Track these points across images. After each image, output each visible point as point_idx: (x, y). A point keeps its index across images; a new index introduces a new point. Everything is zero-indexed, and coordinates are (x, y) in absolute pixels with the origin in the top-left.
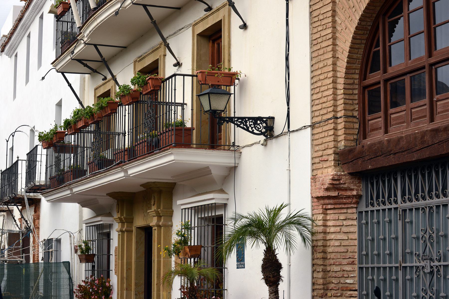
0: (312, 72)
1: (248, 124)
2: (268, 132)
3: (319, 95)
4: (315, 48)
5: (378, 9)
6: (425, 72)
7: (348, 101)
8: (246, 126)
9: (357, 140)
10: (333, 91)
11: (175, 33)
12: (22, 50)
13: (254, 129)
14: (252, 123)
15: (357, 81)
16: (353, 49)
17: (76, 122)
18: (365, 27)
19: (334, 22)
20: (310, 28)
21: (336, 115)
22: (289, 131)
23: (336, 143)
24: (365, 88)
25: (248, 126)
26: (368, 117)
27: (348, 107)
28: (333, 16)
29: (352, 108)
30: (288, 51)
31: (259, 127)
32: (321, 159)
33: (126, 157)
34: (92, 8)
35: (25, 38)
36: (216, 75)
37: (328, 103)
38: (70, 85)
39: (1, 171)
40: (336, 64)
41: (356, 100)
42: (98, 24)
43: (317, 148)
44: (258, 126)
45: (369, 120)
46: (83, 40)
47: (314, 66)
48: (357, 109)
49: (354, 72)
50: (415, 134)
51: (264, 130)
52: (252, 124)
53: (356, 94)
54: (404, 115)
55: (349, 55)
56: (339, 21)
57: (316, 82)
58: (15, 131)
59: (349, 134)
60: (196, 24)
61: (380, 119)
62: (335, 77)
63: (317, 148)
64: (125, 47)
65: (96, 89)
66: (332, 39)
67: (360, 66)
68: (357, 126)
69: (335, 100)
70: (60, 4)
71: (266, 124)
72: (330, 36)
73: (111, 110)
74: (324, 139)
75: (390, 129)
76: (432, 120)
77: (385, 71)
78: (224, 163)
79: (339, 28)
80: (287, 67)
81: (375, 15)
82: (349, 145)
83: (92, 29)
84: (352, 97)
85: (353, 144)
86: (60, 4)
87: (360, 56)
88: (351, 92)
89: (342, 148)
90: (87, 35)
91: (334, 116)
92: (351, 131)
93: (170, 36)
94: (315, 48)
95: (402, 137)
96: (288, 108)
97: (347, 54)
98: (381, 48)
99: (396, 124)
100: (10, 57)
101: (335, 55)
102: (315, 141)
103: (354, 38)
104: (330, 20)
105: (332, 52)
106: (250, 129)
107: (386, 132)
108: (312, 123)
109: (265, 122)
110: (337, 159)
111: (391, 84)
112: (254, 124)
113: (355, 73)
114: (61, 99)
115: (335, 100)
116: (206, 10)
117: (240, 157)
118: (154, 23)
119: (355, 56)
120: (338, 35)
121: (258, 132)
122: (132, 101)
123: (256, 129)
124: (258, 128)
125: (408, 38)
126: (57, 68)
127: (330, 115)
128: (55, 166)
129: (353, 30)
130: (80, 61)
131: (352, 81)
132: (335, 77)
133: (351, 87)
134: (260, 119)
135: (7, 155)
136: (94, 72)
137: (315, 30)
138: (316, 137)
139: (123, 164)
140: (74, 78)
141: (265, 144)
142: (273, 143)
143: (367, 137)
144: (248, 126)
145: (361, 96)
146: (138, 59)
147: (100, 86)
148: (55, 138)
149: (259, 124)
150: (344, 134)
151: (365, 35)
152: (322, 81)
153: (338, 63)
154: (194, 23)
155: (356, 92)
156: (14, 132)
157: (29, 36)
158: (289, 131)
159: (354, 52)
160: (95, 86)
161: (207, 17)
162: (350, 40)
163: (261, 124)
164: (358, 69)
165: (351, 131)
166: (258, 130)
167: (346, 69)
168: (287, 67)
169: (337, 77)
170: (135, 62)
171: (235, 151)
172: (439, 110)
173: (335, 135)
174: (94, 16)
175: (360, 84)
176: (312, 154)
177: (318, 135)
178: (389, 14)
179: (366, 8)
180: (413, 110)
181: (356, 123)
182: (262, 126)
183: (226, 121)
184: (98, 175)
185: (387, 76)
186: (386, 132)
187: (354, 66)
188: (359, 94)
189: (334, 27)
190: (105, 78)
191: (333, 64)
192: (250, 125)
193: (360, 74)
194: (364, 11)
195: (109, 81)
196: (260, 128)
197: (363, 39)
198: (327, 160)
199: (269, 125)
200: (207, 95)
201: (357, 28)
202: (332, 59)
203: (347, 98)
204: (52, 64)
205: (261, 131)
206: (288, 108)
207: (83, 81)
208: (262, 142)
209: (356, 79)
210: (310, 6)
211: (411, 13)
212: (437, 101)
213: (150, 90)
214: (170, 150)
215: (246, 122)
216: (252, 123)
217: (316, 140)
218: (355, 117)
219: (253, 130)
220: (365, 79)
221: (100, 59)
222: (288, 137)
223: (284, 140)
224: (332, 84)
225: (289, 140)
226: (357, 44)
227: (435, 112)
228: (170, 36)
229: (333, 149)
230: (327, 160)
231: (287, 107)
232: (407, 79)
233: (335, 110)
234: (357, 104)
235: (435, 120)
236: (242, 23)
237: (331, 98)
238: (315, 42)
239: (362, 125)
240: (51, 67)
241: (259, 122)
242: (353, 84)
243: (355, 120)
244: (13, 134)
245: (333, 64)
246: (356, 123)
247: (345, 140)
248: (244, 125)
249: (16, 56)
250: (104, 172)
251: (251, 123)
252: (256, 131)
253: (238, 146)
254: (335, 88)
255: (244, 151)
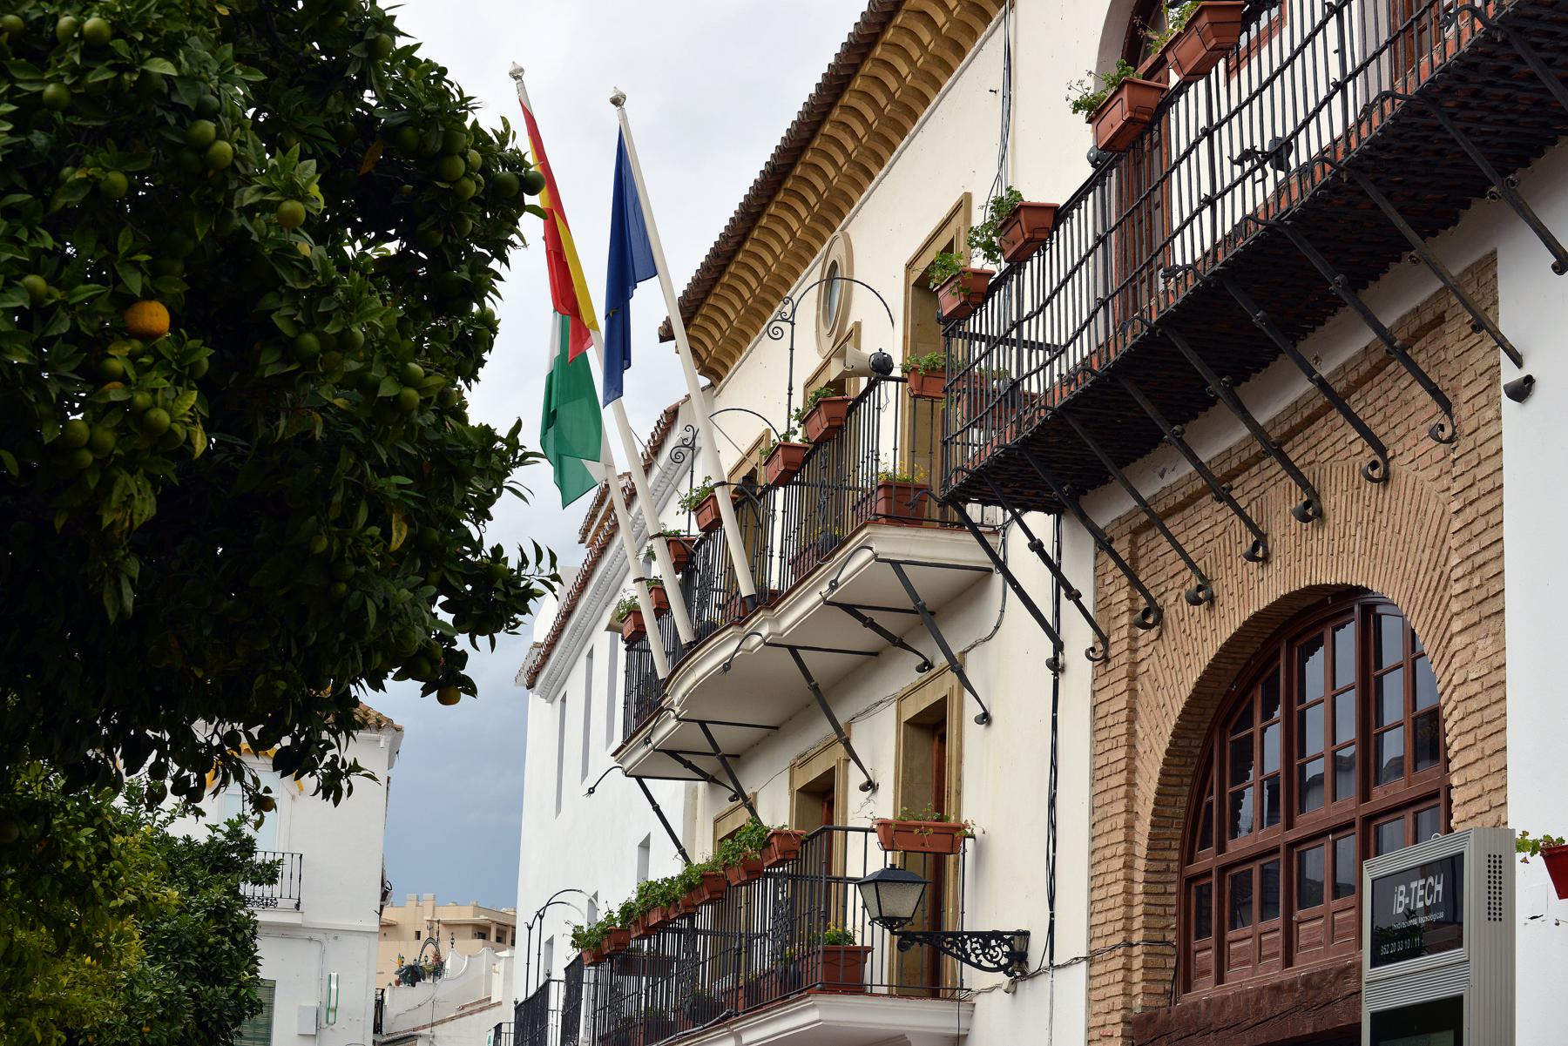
0: (1093, 839)
1: (968, 947)
2: (1016, 964)
3: (1103, 891)
4: (1101, 787)
5: (1212, 712)
6: (1439, 805)
7: (1153, 909)
8: (964, 951)
9: (1172, 993)
10: (1125, 886)
11: (867, 711)
12: (575, 687)
13: (981, 957)
14: (978, 945)
15: (1174, 866)
16: (1163, 797)
17: (645, 914)
18: (1186, 750)
19: (1131, 734)
20: (1092, 742)
21: (1131, 938)
22: (1051, 965)
23: (1127, 998)
24: (1191, 880)
25: (969, 951)
26: (1195, 945)
27: (1154, 922)
28: (1131, 721)
29: (1162, 923)
30: (1055, 788)
31: (995, 954)
32: (1101, 1031)
33: (741, 1003)
34: (683, 642)
35: (583, 659)
36: (916, 831)
37: (1117, 910)
38: (657, 809)
39: (516, 1003)
40: (1133, 827)
41: (1172, 906)
42: (697, 681)
43: (1097, 1008)
44: (992, 952)
45: (1196, 952)
46: (760, 635)
47: (1096, 826)
48: (1174, 926)
49: (1167, 846)
50: (1247, 992)
51: (1004, 961)
52: (977, 948)
53: (1171, 894)
54: (1250, 946)
55: (1154, 810)
56: (1141, 734)
57: (1098, 862)
58: (548, 905)
59: (1154, 980)
60: (903, 697)
61: (1210, 952)
62: (1130, 855)
63: (1097, 1008)
64: (776, 728)
65: (717, 821)
66: (1125, 772)
67: (1180, 832)
68: (1172, 962)
69: (1129, 905)
70: (629, 614)
71: (1011, 947)
72: (1122, 765)
73: (710, 894)
74: (1109, 988)
75: (1227, 974)
76: (1288, 962)
77: (1222, 849)
78: (935, 1028)
79: (1140, 749)
80: (1053, 825)
81: (1206, 726)
82: (1153, 1004)
83: (687, 691)
84: (1162, 900)
85: (1162, 1002)
86: (629, 614)
87: (1181, 812)
88: (1160, 888)
89: (1138, 1010)
90: (679, 702)
91: (1124, 941)
92: (1158, 975)
93: (858, 715)
94: (1101, 787)
95: (1227, 998)
96: (1052, 915)
97: (1152, 806)
98: (1214, 798)
99: (1237, 965)
100: (552, 702)
101: (1133, 806)
102: (1094, 993)
103: (1163, 773)
104: (1123, 729)
105: (1125, 801)
106: (973, 959)
107: (1220, 979)
108: (1091, 952)
109: (1007, 942)
110: (1130, 1033)
111: (1231, 876)
112: (983, 948)
113: (1170, 848)
114: (649, 835)
115: (1129, 905)
116: (920, 669)
117: (971, 1016)
118: (815, 688)
119: (1169, 812)
120: (1138, 763)
121: (991, 965)
122: (746, 878)
123: (986, 959)
124: (991, 956)
125: (1411, 721)
126: (627, 765)
127: (1118, 939)
128: (773, 934)
129: (1161, 755)
130: (850, 609)
131: (1163, 866)
132: (1130, 855)
133: (1162, 878)
134: (997, 935)
135: (539, 954)
136: (895, 645)
137: (1100, 749)
138: (1096, 982)
139: (734, 1018)
140: (671, 793)
141: (1012, 990)
142: (1025, 987)
143: (1193, 988)
144: (969, 951)
145: (1182, 897)
146: (798, 762)
147: (726, 815)
148: (606, 944)
149: (993, 948)
150: (1143, 980)
151: (1190, 766)
152: (1109, 862)
153: (1138, 826)
154: (899, 695)
155: (1173, 888)
156: (545, 908)
157: (590, 655)
158: (1051, 965)
159: (1166, 803)
160: (715, 814)
161: (923, 684)
162: (1156, 776)
163: (999, 946)
164: (1176, 839)
165: (1158, 975)
166: (991, 961)
167: (1150, 839)
168: (1053, 825)
169: (1134, 855)
170: (792, 767)
171: (960, 1000)
172: (1302, 942)
173: (1127, 981)
174: (689, 662)
175: (1180, 872)
176: (1088, 1021)
177: (1099, 979)
178: (1231, 727)
179: (1183, 711)
180: (1263, 938)
181: (1171, 956)
182: (1001, 953)
183: (919, 940)
184: (686, 1040)
185: (1224, 859)
186: (1220, 979)
187: (1168, 833)
188: (1179, 892)
189: (1131, 746)
190: (927, 665)
191: (1126, 827)
192: (973, 950)
193: (1181, 850)
194: (1180, 717)
195: (942, 672)
196: (997, 956)
197: (1186, 776)
198: (1112, 1036)
199: (1017, 949)
200: (873, 885)
201: (1168, 752)
202: (1124, 814)
203: (1153, 901)
204: (614, 754)
205: (998, 963)
206: (1052, 915)
207: (692, 797)
208: (1005, 986)
209: (1173, 861)
210: (1094, 693)
211: (1338, 695)
212: (1299, 923)
213: (775, 859)
214: (810, 999)
215: (964, 942)
216: (978, 945)
217: (1096, 989)
218: (1168, 943)
219: (980, 961)
220: (1190, 861)
221: (910, 605)
222: (1050, 978)
223: (1043, 982)
224: (1123, 871)
225: (1052, 986)
226: (1175, 786)
227: (1295, 946)
228: (858, 715)
229: (1122, 1012)
230: (1112, 1036)
231: (1048, 912)
232: (1256, 868)
233: (1128, 926)
234: (1175, 915)
235: (1295, 963)
236: (866, 780)
237: (1120, 900)
238: (1099, 775)
239: (1182, 961)
240: (612, 762)
241: (993, 943)
242: (1167, 870)
243: (1169, 950)
244: (541, 913)
245: (1126, 827)
246: (1171, 956)
247: (1145, 992)
248: (958, 949)
249: (564, 700)
250: (698, 1035)
251: (974, 946)
252: (985, 963)
253: (969, 990)
254: (1130, 880)
255: (978, 1000)
